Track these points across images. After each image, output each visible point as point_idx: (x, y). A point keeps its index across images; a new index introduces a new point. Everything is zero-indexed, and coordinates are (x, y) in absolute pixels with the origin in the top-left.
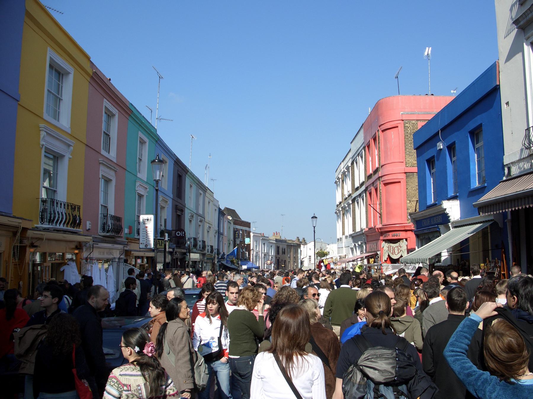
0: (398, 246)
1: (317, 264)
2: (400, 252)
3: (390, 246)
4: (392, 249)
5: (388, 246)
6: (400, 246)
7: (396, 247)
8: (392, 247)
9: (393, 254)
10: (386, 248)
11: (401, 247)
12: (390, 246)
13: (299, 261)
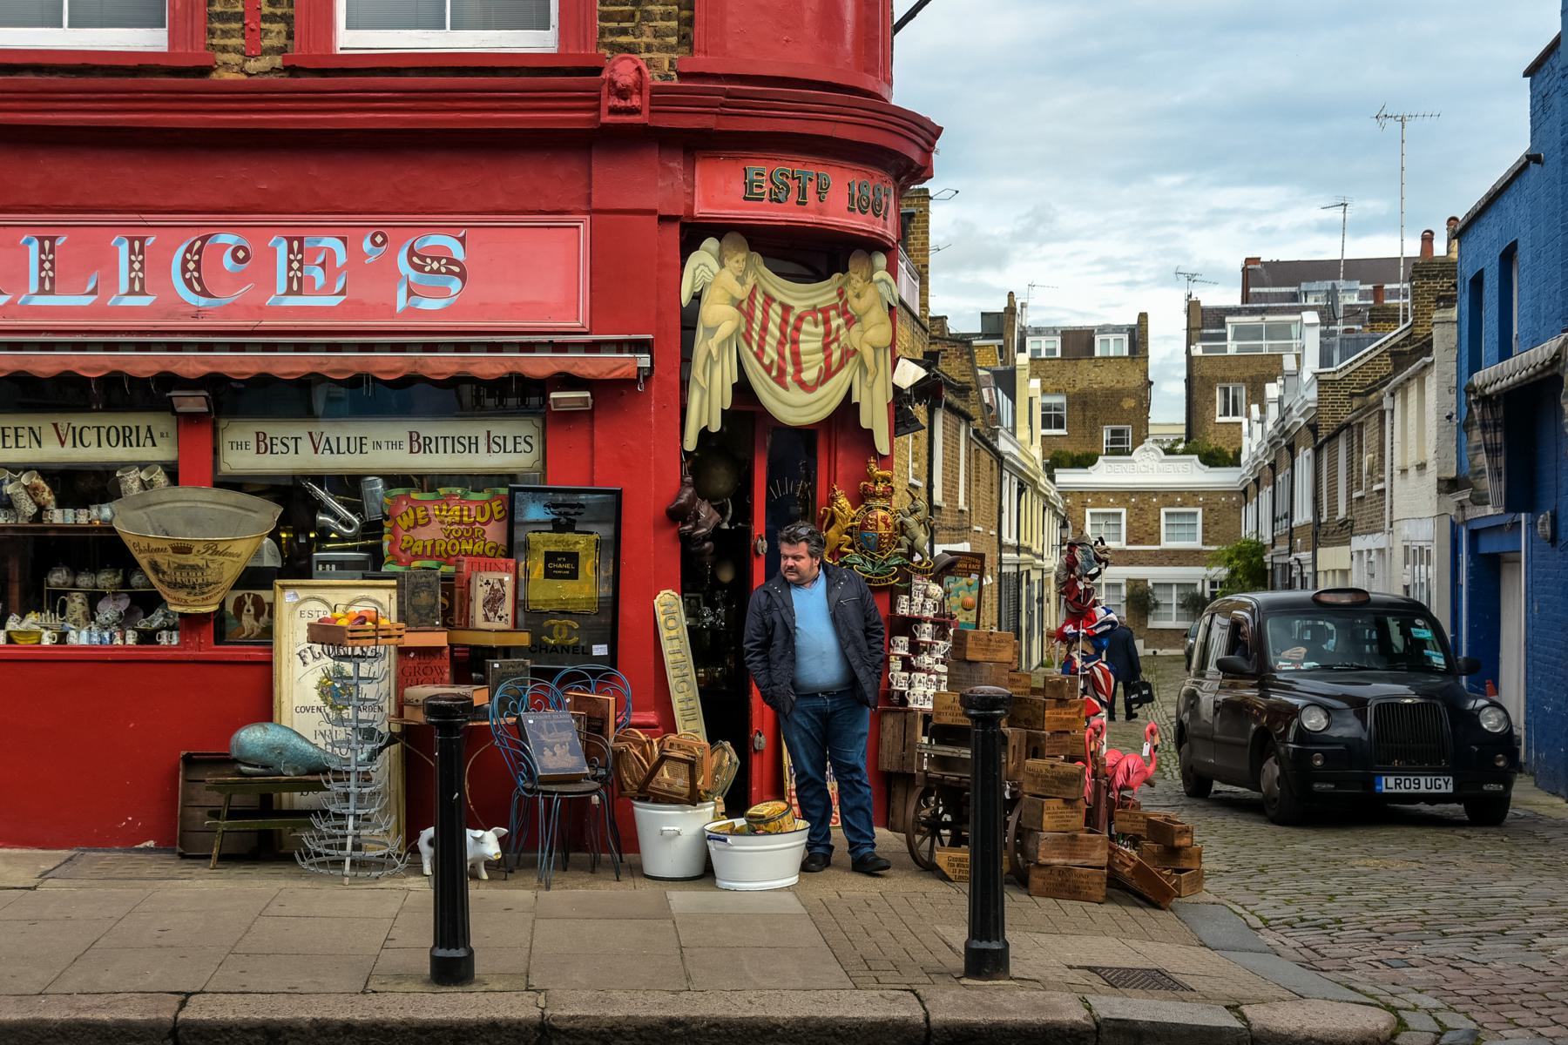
0: (825, 311)
1: (1007, 754)
2: (841, 366)
3: (760, 299)
4: (773, 329)
5: (741, 292)
6: (844, 313)
7: (814, 310)
8: (775, 312)
9: (780, 380)
10: (718, 317)
11: (851, 321)
12: (760, 299)
13: (790, 785)
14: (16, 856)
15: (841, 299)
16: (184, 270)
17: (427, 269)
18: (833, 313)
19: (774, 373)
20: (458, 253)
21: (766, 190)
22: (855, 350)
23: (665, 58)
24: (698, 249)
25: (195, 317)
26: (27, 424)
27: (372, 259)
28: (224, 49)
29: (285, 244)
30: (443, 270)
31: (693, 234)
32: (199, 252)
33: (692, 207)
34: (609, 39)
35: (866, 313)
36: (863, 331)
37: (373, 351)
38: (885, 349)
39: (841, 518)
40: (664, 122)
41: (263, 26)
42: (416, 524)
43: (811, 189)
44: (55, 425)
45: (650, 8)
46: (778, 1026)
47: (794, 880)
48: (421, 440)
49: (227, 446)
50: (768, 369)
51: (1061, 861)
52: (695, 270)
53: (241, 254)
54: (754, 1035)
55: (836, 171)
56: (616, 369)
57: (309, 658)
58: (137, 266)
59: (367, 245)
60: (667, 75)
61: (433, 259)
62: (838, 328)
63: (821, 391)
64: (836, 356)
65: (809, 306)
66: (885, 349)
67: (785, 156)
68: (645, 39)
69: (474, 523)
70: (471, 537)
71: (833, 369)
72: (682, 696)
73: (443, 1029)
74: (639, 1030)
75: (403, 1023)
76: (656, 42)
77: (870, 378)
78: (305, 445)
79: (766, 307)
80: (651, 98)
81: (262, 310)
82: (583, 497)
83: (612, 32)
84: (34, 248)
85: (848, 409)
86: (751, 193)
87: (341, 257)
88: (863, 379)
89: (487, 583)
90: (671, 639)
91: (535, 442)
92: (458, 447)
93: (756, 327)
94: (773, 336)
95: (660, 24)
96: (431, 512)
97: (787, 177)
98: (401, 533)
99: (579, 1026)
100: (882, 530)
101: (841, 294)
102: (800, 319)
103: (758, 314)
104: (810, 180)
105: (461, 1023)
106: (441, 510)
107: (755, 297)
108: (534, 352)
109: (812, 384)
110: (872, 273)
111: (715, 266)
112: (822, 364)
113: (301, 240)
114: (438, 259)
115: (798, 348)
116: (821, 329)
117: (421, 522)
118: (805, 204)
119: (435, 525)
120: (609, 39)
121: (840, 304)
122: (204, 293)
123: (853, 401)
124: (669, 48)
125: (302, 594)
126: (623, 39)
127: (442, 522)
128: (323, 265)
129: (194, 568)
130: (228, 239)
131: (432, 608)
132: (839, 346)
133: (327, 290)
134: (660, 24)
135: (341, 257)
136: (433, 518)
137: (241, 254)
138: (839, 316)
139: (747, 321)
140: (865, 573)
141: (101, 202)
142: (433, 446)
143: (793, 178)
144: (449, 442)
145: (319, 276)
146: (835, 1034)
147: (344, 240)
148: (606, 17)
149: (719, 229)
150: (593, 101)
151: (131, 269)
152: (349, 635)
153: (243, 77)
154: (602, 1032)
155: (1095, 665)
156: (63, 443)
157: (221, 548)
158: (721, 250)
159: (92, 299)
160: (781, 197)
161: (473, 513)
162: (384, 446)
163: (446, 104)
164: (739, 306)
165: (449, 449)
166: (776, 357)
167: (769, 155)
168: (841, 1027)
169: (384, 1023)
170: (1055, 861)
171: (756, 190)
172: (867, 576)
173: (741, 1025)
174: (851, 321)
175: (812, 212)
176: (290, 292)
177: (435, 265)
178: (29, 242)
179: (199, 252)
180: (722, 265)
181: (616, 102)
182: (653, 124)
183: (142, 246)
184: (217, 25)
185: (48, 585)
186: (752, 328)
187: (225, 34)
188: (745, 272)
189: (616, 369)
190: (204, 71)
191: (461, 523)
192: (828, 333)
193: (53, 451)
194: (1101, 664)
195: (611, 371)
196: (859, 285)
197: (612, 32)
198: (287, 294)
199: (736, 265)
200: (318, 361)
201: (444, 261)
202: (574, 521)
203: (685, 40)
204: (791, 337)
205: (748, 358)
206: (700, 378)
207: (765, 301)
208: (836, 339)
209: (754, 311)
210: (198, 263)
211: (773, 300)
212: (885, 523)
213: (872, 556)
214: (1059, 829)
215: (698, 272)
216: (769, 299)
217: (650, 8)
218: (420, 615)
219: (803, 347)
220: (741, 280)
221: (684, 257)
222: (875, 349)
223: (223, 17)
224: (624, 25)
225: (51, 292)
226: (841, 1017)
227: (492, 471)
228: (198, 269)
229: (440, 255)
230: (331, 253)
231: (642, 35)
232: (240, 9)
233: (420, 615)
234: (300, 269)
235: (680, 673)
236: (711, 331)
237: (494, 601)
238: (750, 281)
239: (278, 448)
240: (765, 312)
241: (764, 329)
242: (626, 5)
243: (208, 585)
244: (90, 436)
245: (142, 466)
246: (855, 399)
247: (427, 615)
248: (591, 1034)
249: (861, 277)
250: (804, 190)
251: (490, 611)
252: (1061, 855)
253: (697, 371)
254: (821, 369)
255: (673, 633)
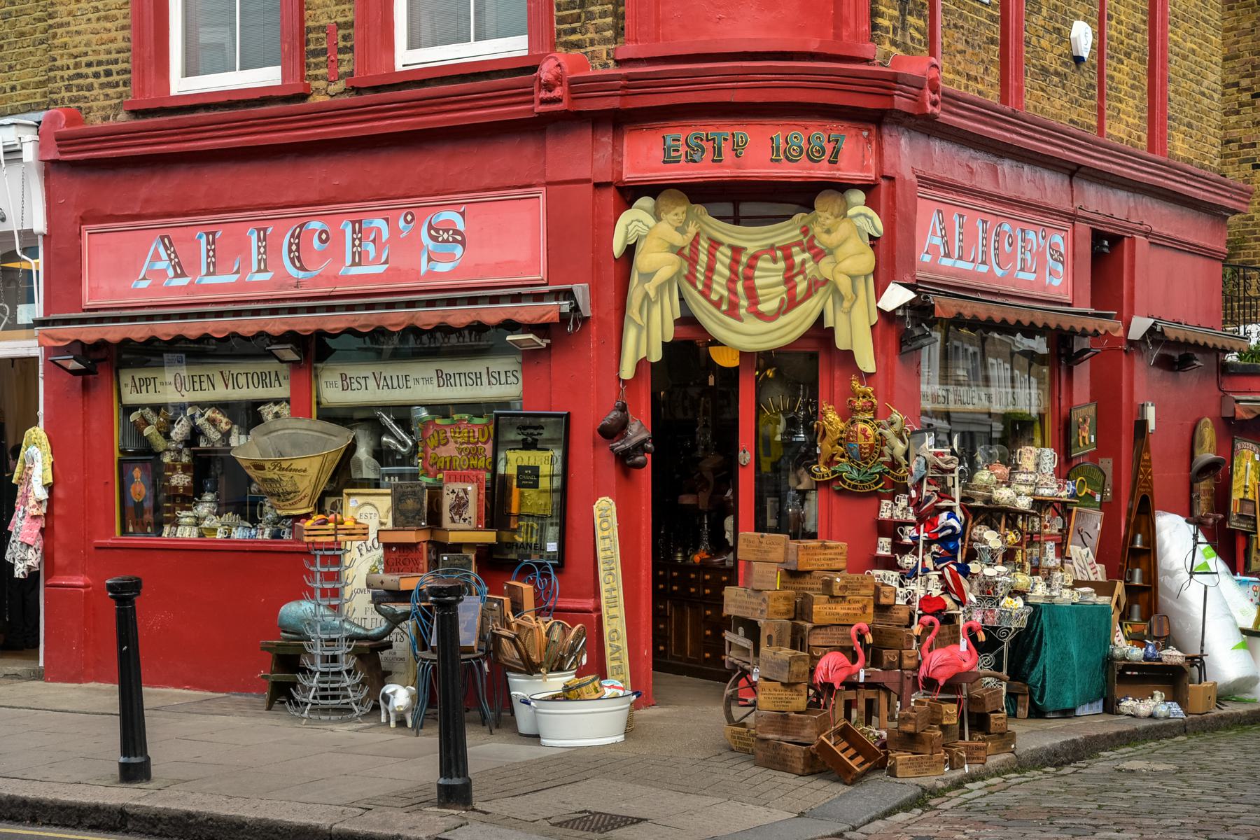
3: (704, 244)
6: (811, 247)
8: (723, 256)
9: (733, 310)
11: (818, 255)
12: (704, 244)
14: (71, 688)
15: (805, 236)
16: (290, 251)
17: (440, 239)
18: (795, 249)
19: (724, 307)
20: (461, 226)
21: (682, 152)
22: (827, 281)
23: (602, 49)
24: (630, 208)
25: (297, 287)
26: (205, 373)
27: (404, 234)
28: (316, 78)
29: (350, 226)
30: (451, 239)
31: (629, 194)
32: (298, 237)
33: (621, 173)
34: (564, 38)
35: (838, 246)
36: (836, 263)
37: (414, 307)
38: (866, 277)
39: (830, 430)
40: (584, 106)
41: (340, 57)
42: (439, 444)
43: (726, 148)
44: (222, 373)
45: (592, 9)
46: (245, 823)
47: (620, 738)
48: (444, 376)
49: (324, 385)
50: (717, 305)
51: (776, 736)
52: (627, 226)
53: (324, 236)
54: (232, 829)
55: (756, 129)
56: (544, 315)
57: (364, 551)
58: (262, 250)
59: (402, 223)
60: (606, 64)
61: (444, 231)
62: (803, 262)
63: (783, 320)
64: (802, 287)
65: (766, 245)
66: (866, 277)
67: (699, 122)
68: (589, 35)
69: (477, 443)
70: (475, 454)
71: (798, 299)
72: (608, 586)
73: (71, 808)
74: (171, 818)
75: (52, 802)
76: (596, 37)
77: (846, 304)
78: (371, 383)
79: (712, 250)
80: (569, 88)
81: (337, 279)
82: (543, 420)
83: (566, 32)
84: (203, 241)
85: (821, 333)
86: (669, 156)
87: (385, 235)
88: (838, 306)
89: (453, 492)
90: (604, 538)
91: (520, 376)
92: (469, 381)
93: (701, 268)
94: (721, 275)
95: (599, 21)
96: (449, 434)
97: (702, 140)
98: (430, 451)
99: (139, 812)
100: (861, 441)
101: (805, 231)
102: (755, 257)
103: (703, 258)
104: (725, 139)
105: (81, 804)
106: (455, 433)
107: (698, 243)
108: (498, 303)
109: (772, 314)
110: (846, 209)
111: (650, 221)
112: (785, 296)
113: (360, 222)
114: (447, 231)
115: (754, 283)
116: (782, 265)
117: (443, 442)
118: (721, 161)
119: (452, 445)
120: (564, 38)
121: (805, 240)
122: (302, 268)
123: (826, 326)
124: (606, 41)
125: (360, 500)
126: (574, 38)
127: (456, 442)
128: (374, 241)
129: (272, 480)
130: (316, 225)
131: (419, 512)
132: (805, 278)
133: (376, 261)
134: (599, 21)
135: (385, 235)
136: (450, 439)
137: (324, 236)
138: (803, 251)
139: (690, 265)
140: (852, 480)
141: (240, 203)
142: (452, 380)
143: (708, 140)
144: (462, 377)
145: (371, 248)
146: (277, 832)
147: (387, 220)
148: (562, 20)
149: (654, 190)
150: (526, 94)
151: (259, 253)
152: (306, 533)
153: (327, 98)
154: (151, 818)
155: (947, 566)
156: (227, 386)
157: (285, 465)
158: (656, 207)
159: (237, 276)
160: (696, 157)
161: (477, 434)
162: (421, 381)
163: (436, 108)
164: (679, 252)
165: (463, 383)
166: (726, 293)
167: (684, 122)
168: (281, 828)
169: (42, 801)
170: (770, 736)
171: (673, 154)
172: (853, 483)
173: (225, 820)
174: (818, 255)
175: (728, 167)
176: (354, 264)
177: (446, 236)
178: (200, 237)
179: (298, 237)
180: (658, 218)
181: (544, 94)
182: (571, 110)
183: (265, 234)
184: (312, 60)
185: (250, 493)
186: (696, 270)
187: (317, 66)
188: (686, 223)
189: (544, 315)
190: (303, 97)
191: (469, 443)
192: (790, 267)
193: (221, 392)
194: (951, 566)
195: (541, 317)
196: (828, 221)
197: (566, 32)
198: (257, 272)
199: (675, 218)
200: (353, 318)
201: (451, 232)
202: (537, 440)
203: (619, 31)
204: (744, 274)
205: (693, 297)
206: (637, 317)
207: (711, 246)
208: (802, 272)
209: (697, 255)
210: (298, 245)
211: (721, 244)
212: (864, 434)
213: (858, 465)
214: (777, 709)
215: (630, 228)
216: (715, 244)
217: (592, 9)
218: (407, 517)
219: (758, 282)
220: (681, 230)
221: (616, 219)
222: (853, 278)
223: (316, 53)
224: (574, 25)
225: (214, 274)
226: (281, 821)
227: (388, 403)
228: (298, 250)
229: (449, 227)
230: (379, 230)
231: (587, 32)
232: (325, 46)
233: (408, 517)
234: (360, 245)
235: (608, 567)
236: (648, 277)
237: (459, 506)
238: (692, 230)
239: (355, 385)
240: (712, 256)
241: (711, 269)
242: (575, 8)
243: (289, 493)
244: (242, 380)
245: (277, 402)
246: (828, 323)
247: (414, 517)
248: (145, 818)
249: (832, 214)
250: (720, 149)
251: (456, 514)
252: (775, 731)
253: (633, 310)
254: (782, 301)
255: (606, 533)
